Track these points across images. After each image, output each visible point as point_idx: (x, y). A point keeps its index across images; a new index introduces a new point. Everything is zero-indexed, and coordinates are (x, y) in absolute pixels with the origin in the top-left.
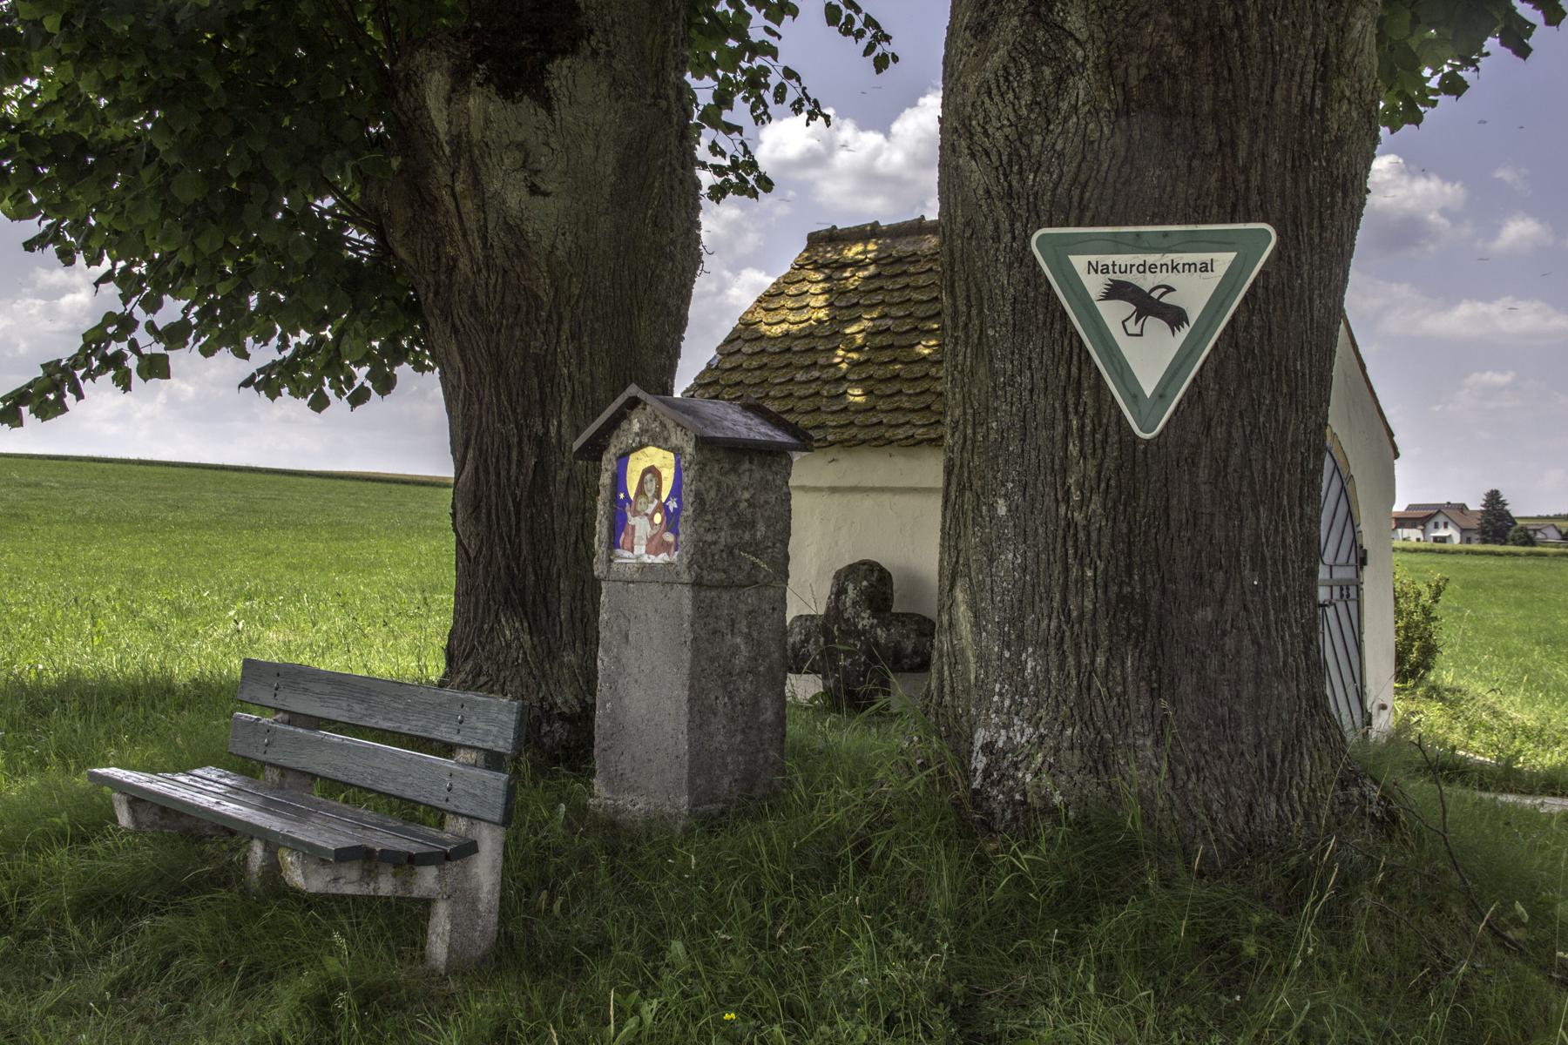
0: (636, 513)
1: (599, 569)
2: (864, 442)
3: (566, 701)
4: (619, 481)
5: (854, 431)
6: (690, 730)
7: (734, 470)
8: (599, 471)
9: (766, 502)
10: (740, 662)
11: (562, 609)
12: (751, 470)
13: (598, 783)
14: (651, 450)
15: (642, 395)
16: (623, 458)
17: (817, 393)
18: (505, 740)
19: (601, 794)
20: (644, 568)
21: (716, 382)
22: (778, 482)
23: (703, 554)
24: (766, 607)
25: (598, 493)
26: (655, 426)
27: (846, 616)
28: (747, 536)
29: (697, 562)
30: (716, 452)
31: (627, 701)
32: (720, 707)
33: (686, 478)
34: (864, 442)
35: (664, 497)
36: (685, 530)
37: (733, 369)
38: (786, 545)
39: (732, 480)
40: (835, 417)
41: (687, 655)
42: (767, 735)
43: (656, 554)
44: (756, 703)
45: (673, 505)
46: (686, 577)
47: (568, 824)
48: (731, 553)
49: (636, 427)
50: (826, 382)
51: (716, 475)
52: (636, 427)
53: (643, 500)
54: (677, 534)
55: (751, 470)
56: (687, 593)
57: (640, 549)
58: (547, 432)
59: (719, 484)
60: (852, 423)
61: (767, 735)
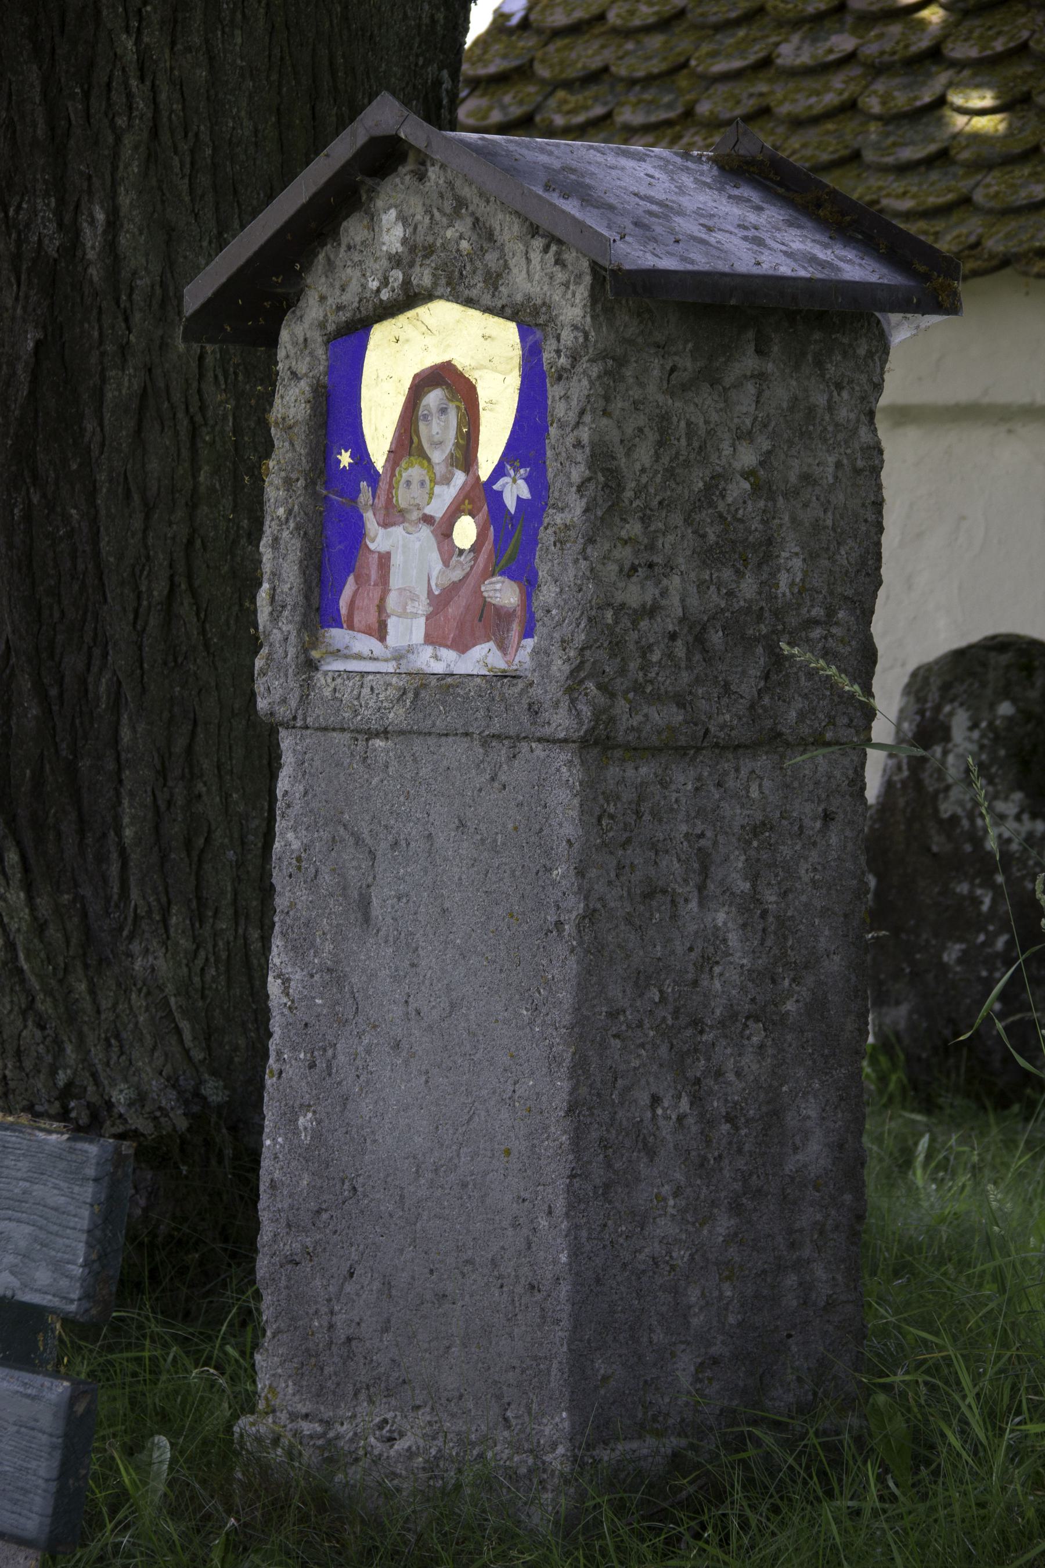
0: (392, 515)
1: (272, 691)
2: (1005, 262)
3: (140, 1099)
4: (337, 406)
5: (971, 227)
6: (575, 1202)
7: (710, 376)
8: (270, 379)
9: (807, 478)
10: (725, 986)
11: (127, 810)
12: (760, 377)
13: (269, 1365)
14: (441, 313)
15: (414, 131)
16: (350, 338)
17: (850, 107)
18: (57, 1266)
19: (282, 1404)
20: (420, 688)
21: (522, 73)
22: (843, 414)
23: (616, 647)
24: (807, 811)
25: (267, 448)
26: (457, 234)
27: (946, 809)
28: (748, 587)
29: (596, 673)
30: (660, 320)
31: (366, 1107)
32: (666, 1129)
33: (562, 403)
34: (1005, 262)
35: (489, 453)
36: (558, 574)
37: (575, 29)
38: (866, 614)
39: (701, 409)
40: (911, 183)
41: (563, 966)
42: (808, 1216)
43: (462, 646)
44: (775, 1114)
45: (514, 490)
46: (560, 721)
47: (180, 1502)
48: (700, 640)
49: (392, 235)
50: (877, 70)
51: (652, 390)
52: (392, 235)
53: (414, 472)
54: (529, 583)
55: (760, 377)
56: (564, 770)
57: (407, 630)
58: (73, 245)
59: (663, 422)
60: (966, 201)
61: (808, 1216)
